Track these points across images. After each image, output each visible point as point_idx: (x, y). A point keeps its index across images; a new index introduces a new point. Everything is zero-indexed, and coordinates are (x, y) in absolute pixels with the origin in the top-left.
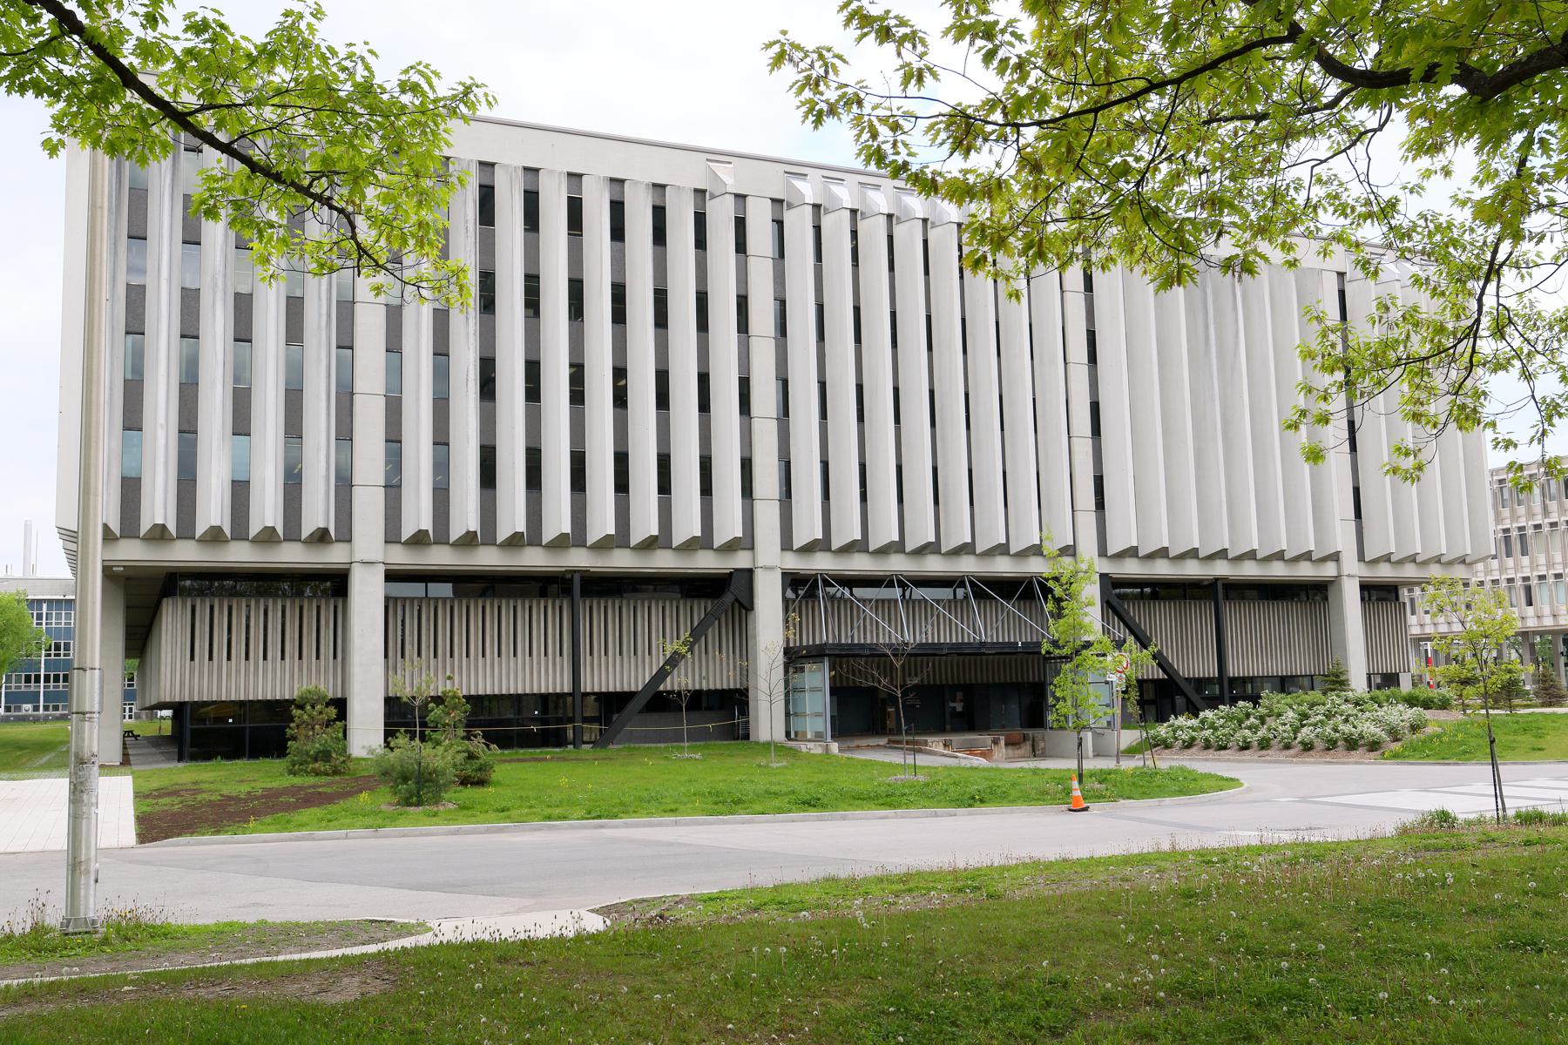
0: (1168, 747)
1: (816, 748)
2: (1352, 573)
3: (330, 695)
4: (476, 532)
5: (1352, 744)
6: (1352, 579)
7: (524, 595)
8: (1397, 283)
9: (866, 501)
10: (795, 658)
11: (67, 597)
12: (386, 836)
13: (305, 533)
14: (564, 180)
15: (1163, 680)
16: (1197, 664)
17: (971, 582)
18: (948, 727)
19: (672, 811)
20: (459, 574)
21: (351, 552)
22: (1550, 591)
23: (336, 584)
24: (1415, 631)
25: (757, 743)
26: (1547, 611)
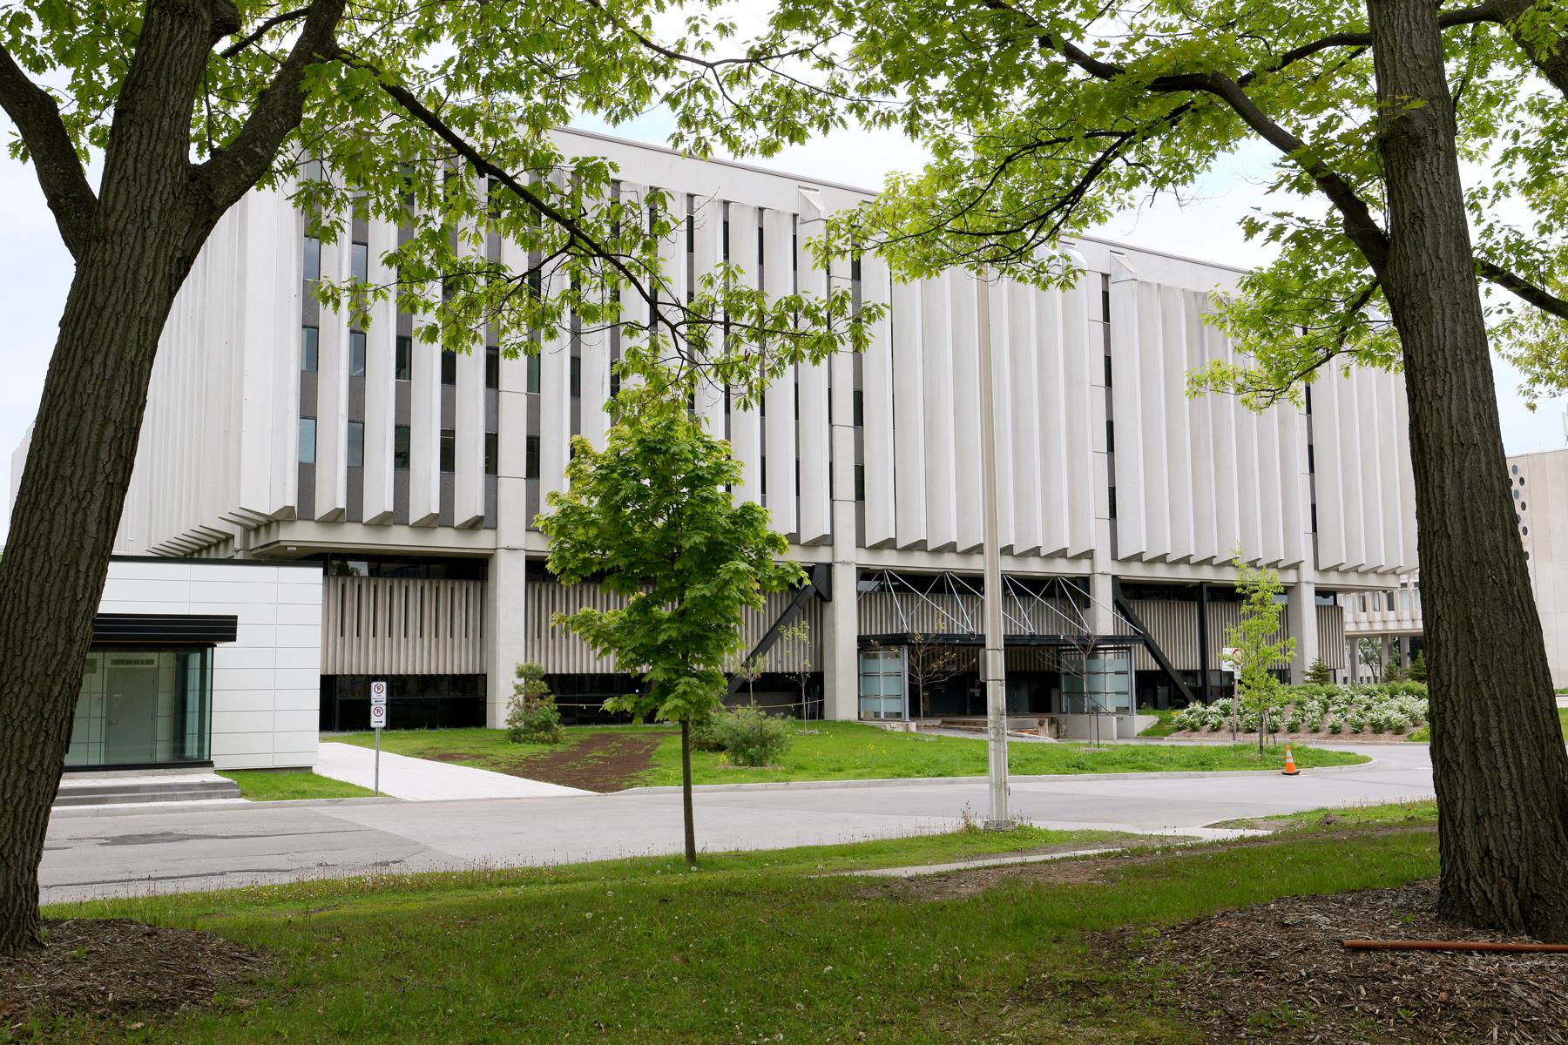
0: (1194, 729)
1: (897, 727)
2: (1105, 571)
5: (1378, 728)
6: (846, 568)
7: (428, 575)
9: (863, 498)
10: (865, 645)
12: (795, 789)
13: (319, 514)
15: (1156, 671)
16: (1183, 658)
17: (890, 575)
18: (968, 711)
21: (1298, 575)
24: (1350, 628)
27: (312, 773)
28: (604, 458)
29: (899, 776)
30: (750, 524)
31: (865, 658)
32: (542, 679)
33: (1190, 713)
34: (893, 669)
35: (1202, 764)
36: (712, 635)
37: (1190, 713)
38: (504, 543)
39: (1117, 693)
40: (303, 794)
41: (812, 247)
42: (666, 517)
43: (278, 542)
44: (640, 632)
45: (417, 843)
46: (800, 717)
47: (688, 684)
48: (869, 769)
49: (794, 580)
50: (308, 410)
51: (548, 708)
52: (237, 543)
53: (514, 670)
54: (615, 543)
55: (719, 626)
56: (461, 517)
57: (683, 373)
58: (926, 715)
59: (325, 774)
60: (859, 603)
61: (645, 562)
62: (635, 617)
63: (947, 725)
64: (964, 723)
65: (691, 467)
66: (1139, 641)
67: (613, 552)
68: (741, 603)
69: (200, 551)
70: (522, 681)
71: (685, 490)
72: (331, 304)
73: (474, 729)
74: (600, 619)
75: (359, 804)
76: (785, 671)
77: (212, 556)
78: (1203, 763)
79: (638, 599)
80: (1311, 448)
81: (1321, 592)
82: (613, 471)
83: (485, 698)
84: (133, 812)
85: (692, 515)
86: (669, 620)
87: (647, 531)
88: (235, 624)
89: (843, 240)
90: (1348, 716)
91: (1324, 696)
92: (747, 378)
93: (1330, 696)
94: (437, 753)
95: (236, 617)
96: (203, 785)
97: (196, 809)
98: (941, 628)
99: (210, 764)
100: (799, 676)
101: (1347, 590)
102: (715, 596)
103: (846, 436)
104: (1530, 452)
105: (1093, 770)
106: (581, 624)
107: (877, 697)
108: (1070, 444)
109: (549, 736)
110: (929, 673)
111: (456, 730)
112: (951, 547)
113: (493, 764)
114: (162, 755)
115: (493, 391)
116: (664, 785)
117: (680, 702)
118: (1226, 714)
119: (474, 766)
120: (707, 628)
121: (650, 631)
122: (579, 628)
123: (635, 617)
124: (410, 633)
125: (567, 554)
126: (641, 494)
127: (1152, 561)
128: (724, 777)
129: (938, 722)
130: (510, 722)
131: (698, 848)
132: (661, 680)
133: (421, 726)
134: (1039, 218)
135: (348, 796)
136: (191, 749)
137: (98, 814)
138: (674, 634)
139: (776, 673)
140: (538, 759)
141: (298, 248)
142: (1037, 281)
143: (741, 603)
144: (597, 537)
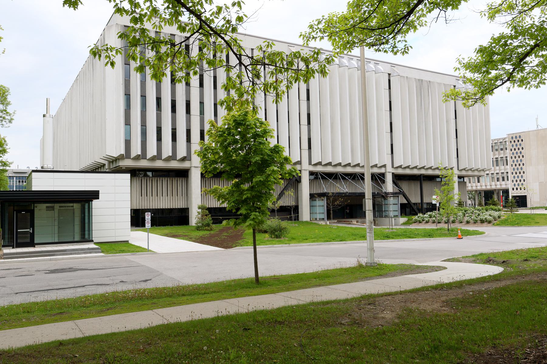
0: (420, 222)
1: (323, 223)
2: (390, 171)
3: (207, 207)
4: (124, 154)
5: (482, 221)
6: (390, 173)
8: (464, 88)
10: (312, 197)
11: (9, 175)
14: (250, 50)
15: (406, 204)
16: (415, 199)
17: (320, 174)
18: (345, 217)
19: (355, 239)
20: (155, 169)
21: (386, 170)
22: (485, 178)
23: (184, 174)
24: (470, 188)
25: (302, 222)
26: (484, 184)
27: (129, 243)
28: (221, 128)
29: (327, 241)
30: (278, 152)
31: (312, 201)
32: (206, 210)
33: (418, 217)
34: (321, 205)
35: (429, 235)
36: (264, 195)
37: (418, 217)
38: (193, 165)
39: (394, 211)
40: (123, 251)
41: (302, 37)
42: (245, 151)
43: (119, 166)
44: (236, 195)
45: (158, 271)
46: (291, 220)
47: (255, 215)
48: (317, 239)
49: (294, 174)
50: (128, 122)
51: (209, 219)
52: (107, 167)
53: (197, 206)
54: (226, 161)
55: (266, 192)
56: (179, 156)
57: (250, 89)
58: (334, 219)
59: (133, 244)
60: (310, 183)
61: (237, 168)
62: (234, 189)
63: (339, 222)
64: (344, 221)
65: (254, 130)
66: (401, 194)
67: (225, 164)
68: (275, 183)
69: (98, 168)
70: (200, 210)
71: (252, 140)
72: (97, 56)
73: (185, 226)
74: (221, 190)
75: (142, 255)
76: (286, 205)
77: (99, 170)
78: (429, 235)
79: (235, 182)
80: (456, 130)
81: (460, 177)
82: (225, 133)
83: (188, 216)
84: (63, 259)
85: (255, 150)
86: (247, 190)
87: (238, 156)
88: (99, 193)
89: (315, 33)
90: (472, 218)
91: (464, 211)
92: (277, 91)
93: (465, 211)
94: (172, 234)
95: (99, 191)
96: (89, 249)
97: (85, 257)
98: (338, 191)
99: (92, 241)
100: (291, 207)
101: (468, 176)
102: (265, 181)
103: (305, 128)
104: (525, 131)
105: (393, 238)
106: (213, 192)
107: (316, 213)
108: (378, 130)
109: (209, 228)
110: (334, 205)
111: (179, 226)
112: (339, 164)
113: (190, 238)
114: (77, 238)
115: (188, 115)
116: (247, 246)
117: (252, 222)
118: (431, 217)
119: (183, 239)
120: (261, 193)
121: (240, 194)
122: (212, 194)
123: (234, 189)
124: (164, 195)
125: (208, 165)
126: (236, 142)
127: (405, 168)
128: (268, 243)
129: (336, 221)
130: (196, 224)
131: (260, 275)
132: (244, 213)
133: (168, 225)
134: (396, 22)
135: (139, 252)
136: (86, 236)
137: (51, 260)
138: (249, 195)
139: (283, 206)
140: (205, 236)
141: (122, 68)
142: (392, 51)
143: (275, 183)
144: (218, 158)
